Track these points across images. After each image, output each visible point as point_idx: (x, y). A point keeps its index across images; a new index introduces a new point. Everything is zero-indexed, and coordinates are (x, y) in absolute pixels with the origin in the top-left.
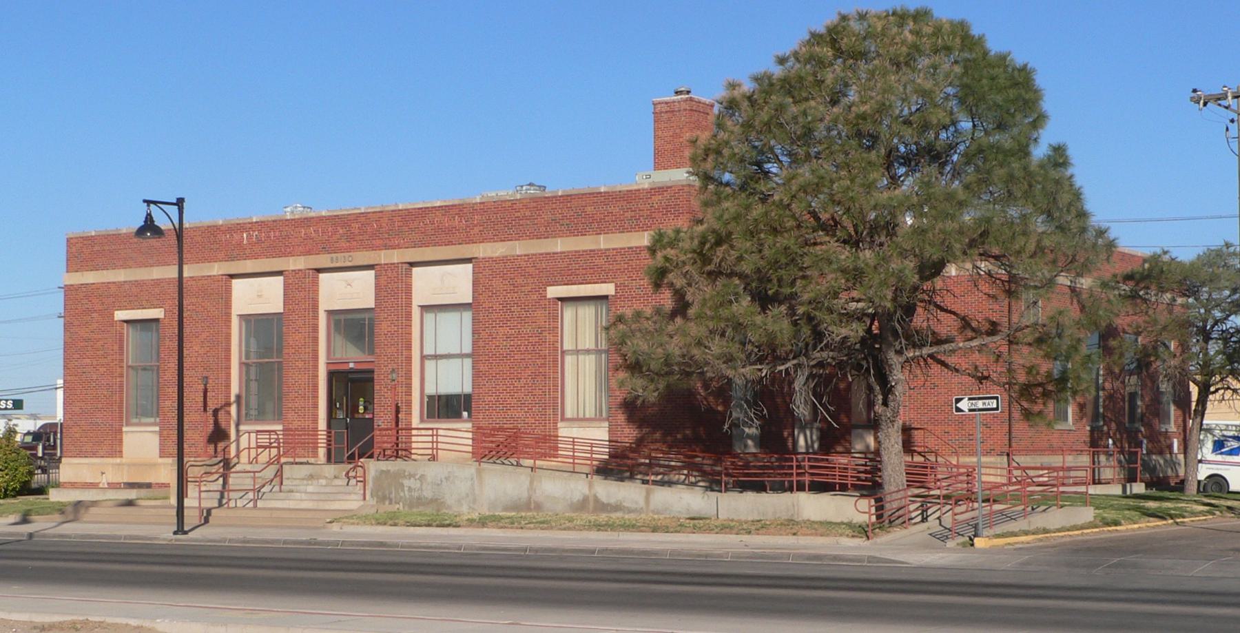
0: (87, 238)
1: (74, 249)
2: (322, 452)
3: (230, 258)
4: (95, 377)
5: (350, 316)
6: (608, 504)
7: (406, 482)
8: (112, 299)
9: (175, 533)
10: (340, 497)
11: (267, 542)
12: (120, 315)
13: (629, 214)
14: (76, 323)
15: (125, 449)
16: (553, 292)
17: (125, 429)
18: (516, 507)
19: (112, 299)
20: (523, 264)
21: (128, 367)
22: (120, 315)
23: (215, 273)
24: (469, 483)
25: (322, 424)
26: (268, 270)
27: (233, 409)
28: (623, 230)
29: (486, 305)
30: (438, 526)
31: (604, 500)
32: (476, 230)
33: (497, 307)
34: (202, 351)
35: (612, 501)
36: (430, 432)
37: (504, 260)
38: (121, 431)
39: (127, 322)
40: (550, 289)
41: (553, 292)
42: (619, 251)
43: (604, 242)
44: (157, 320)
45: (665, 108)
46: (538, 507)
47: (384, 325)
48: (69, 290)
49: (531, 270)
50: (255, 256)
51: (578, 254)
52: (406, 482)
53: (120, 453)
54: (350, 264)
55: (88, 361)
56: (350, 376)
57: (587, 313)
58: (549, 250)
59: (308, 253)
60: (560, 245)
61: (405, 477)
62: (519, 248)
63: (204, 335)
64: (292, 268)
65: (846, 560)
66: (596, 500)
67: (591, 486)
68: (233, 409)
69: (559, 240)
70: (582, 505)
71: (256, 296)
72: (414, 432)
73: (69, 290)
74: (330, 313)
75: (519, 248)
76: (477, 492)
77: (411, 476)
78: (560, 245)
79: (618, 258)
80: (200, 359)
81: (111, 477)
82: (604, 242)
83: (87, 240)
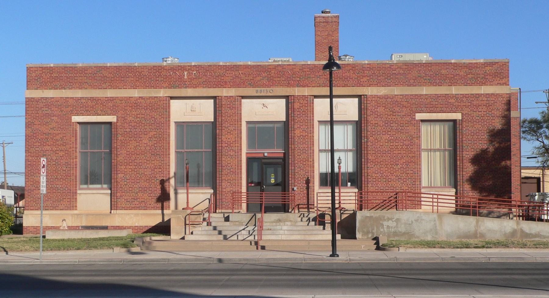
0: (46, 68)
1: (34, 75)
2: (244, 206)
3: (170, 87)
4: (54, 158)
5: (261, 125)
6: (531, 234)
7: (385, 223)
8: (70, 109)
9: (331, 256)
10: (315, 232)
11: (429, 259)
12: (76, 119)
13: (470, 76)
14: (37, 122)
15: (78, 205)
16: (419, 116)
17: (79, 192)
18: (467, 236)
19: (70, 109)
20: (399, 100)
21: (320, 151)
22: (76, 119)
23: (161, 95)
24: (433, 223)
25: (244, 189)
26: (197, 95)
27: (172, 181)
28: (466, 84)
29: (374, 122)
30: (475, 247)
31: (528, 231)
32: (365, 79)
33: (381, 123)
34: (151, 143)
35: (533, 232)
36: (431, 196)
37: (386, 97)
38: (76, 193)
39: (79, 123)
40: (417, 115)
41: (419, 116)
42: (464, 96)
43: (454, 90)
44: (110, 123)
45: (323, 20)
46: (482, 235)
47: (297, 132)
48: (29, 102)
49: (405, 104)
50: (195, 86)
51: (438, 96)
52: (385, 223)
53: (74, 207)
54: (271, 94)
55: (48, 148)
56: (263, 161)
57: (437, 127)
58: (417, 93)
59: (238, 86)
60: (425, 90)
61: (385, 220)
62: (397, 91)
63: (152, 134)
64: (225, 95)
65: (114, 262)
66: (522, 231)
67: (518, 224)
68: (172, 181)
69: (424, 88)
70: (514, 233)
71: (192, 110)
72: (422, 195)
73: (29, 102)
74: (248, 123)
75: (397, 91)
76: (438, 228)
77: (389, 219)
78: (425, 90)
79: (465, 99)
80: (148, 148)
81: (70, 222)
82: (454, 90)
83: (44, 69)
